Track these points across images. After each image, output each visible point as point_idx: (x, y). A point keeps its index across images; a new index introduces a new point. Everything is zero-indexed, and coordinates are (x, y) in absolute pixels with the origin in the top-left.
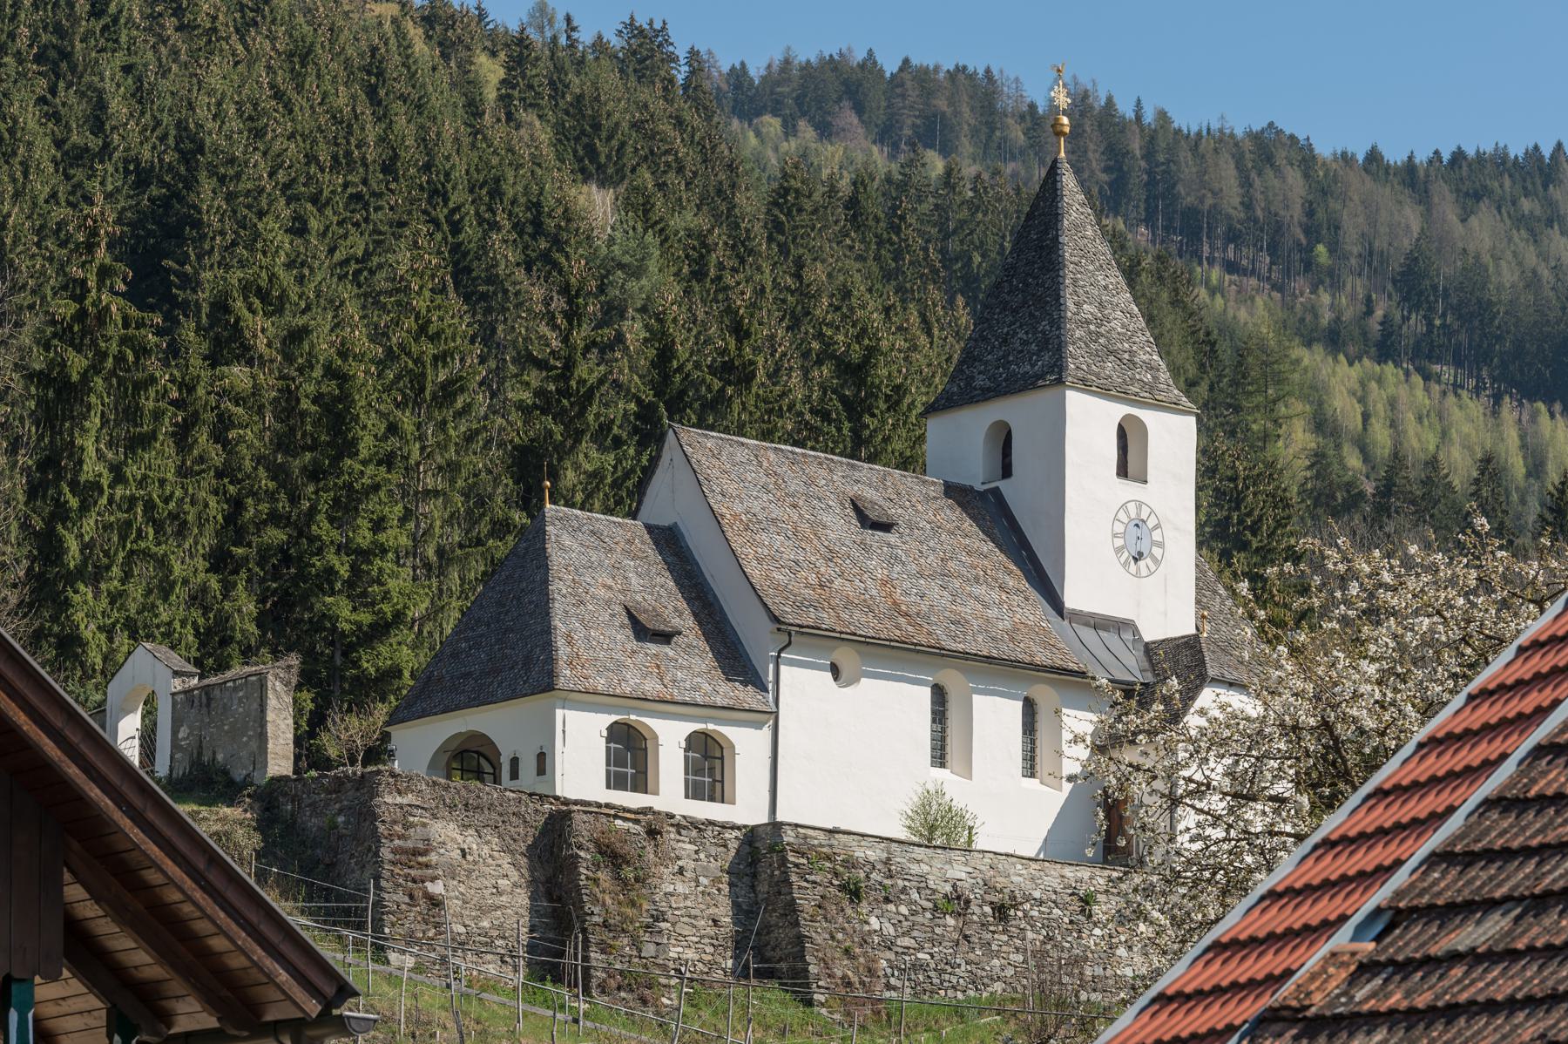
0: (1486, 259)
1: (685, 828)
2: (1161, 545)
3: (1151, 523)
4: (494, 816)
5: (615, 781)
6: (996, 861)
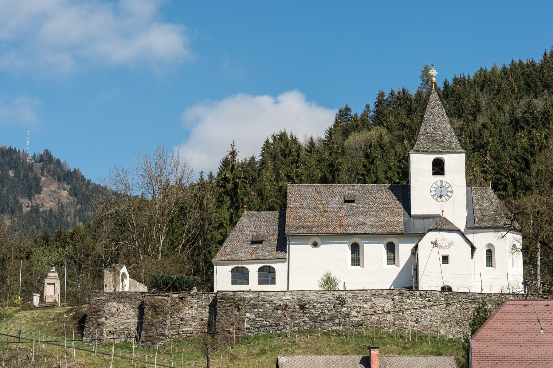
0: (61, 177)
1: (194, 295)
2: (452, 192)
3: (447, 186)
4: (129, 299)
5: (234, 283)
6: (304, 293)
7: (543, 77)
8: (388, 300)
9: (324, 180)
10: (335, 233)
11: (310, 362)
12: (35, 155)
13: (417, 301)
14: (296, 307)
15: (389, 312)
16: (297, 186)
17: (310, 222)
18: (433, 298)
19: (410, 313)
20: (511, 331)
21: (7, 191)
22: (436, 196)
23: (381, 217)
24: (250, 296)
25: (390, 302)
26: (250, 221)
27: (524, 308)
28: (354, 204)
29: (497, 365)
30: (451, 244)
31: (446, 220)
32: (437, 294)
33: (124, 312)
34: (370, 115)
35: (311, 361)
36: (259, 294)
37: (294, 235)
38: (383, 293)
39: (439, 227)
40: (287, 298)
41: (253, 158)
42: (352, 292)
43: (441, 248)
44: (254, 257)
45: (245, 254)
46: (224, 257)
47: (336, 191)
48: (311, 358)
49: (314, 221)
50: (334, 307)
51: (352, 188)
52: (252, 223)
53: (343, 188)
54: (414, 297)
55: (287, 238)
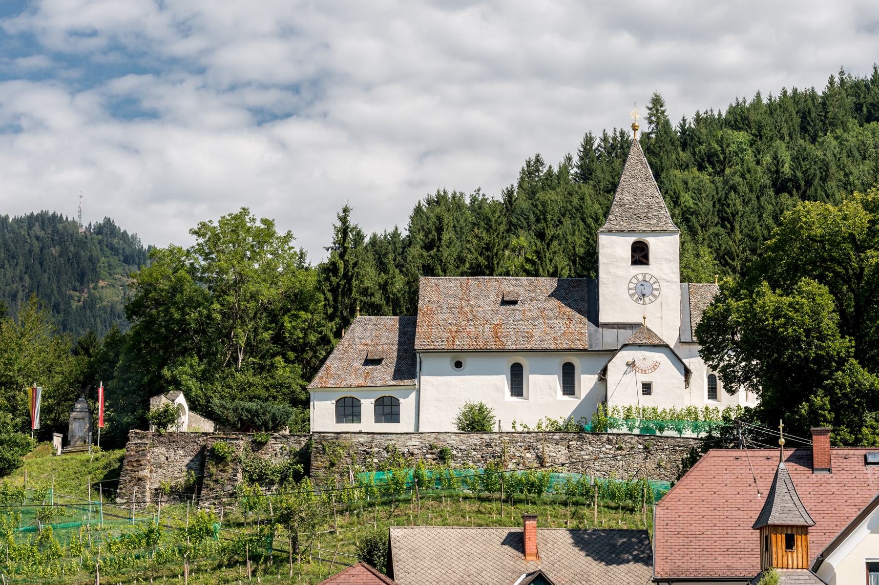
1: (279, 438)
2: (659, 289)
3: (651, 282)
5: (339, 420)
7: (826, 117)
8: (561, 447)
9: (476, 271)
11: (436, 537)
12: (90, 225)
13: (604, 449)
14: (427, 456)
15: (563, 465)
16: (433, 280)
17: (451, 332)
20: (715, 495)
21: (49, 279)
22: (636, 296)
24: (360, 439)
25: (564, 450)
26: (365, 330)
27: (735, 462)
28: (516, 307)
29: (691, 544)
30: (655, 366)
31: (649, 331)
32: (632, 438)
33: (177, 461)
34: (572, 172)
35: (439, 535)
36: (373, 438)
37: (426, 351)
38: (554, 437)
40: (414, 443)
41: (395, 234)
43: (640, 371)
44: (369, 384)
45: (357, 378)
46: (325, 382)
47: (492, 288)
48: (439, 531)
49: (456, 332)
50: (482, 457)
51: (514, 283)
52: (368, 334)
53: (502, 283)
55: (418, 355)
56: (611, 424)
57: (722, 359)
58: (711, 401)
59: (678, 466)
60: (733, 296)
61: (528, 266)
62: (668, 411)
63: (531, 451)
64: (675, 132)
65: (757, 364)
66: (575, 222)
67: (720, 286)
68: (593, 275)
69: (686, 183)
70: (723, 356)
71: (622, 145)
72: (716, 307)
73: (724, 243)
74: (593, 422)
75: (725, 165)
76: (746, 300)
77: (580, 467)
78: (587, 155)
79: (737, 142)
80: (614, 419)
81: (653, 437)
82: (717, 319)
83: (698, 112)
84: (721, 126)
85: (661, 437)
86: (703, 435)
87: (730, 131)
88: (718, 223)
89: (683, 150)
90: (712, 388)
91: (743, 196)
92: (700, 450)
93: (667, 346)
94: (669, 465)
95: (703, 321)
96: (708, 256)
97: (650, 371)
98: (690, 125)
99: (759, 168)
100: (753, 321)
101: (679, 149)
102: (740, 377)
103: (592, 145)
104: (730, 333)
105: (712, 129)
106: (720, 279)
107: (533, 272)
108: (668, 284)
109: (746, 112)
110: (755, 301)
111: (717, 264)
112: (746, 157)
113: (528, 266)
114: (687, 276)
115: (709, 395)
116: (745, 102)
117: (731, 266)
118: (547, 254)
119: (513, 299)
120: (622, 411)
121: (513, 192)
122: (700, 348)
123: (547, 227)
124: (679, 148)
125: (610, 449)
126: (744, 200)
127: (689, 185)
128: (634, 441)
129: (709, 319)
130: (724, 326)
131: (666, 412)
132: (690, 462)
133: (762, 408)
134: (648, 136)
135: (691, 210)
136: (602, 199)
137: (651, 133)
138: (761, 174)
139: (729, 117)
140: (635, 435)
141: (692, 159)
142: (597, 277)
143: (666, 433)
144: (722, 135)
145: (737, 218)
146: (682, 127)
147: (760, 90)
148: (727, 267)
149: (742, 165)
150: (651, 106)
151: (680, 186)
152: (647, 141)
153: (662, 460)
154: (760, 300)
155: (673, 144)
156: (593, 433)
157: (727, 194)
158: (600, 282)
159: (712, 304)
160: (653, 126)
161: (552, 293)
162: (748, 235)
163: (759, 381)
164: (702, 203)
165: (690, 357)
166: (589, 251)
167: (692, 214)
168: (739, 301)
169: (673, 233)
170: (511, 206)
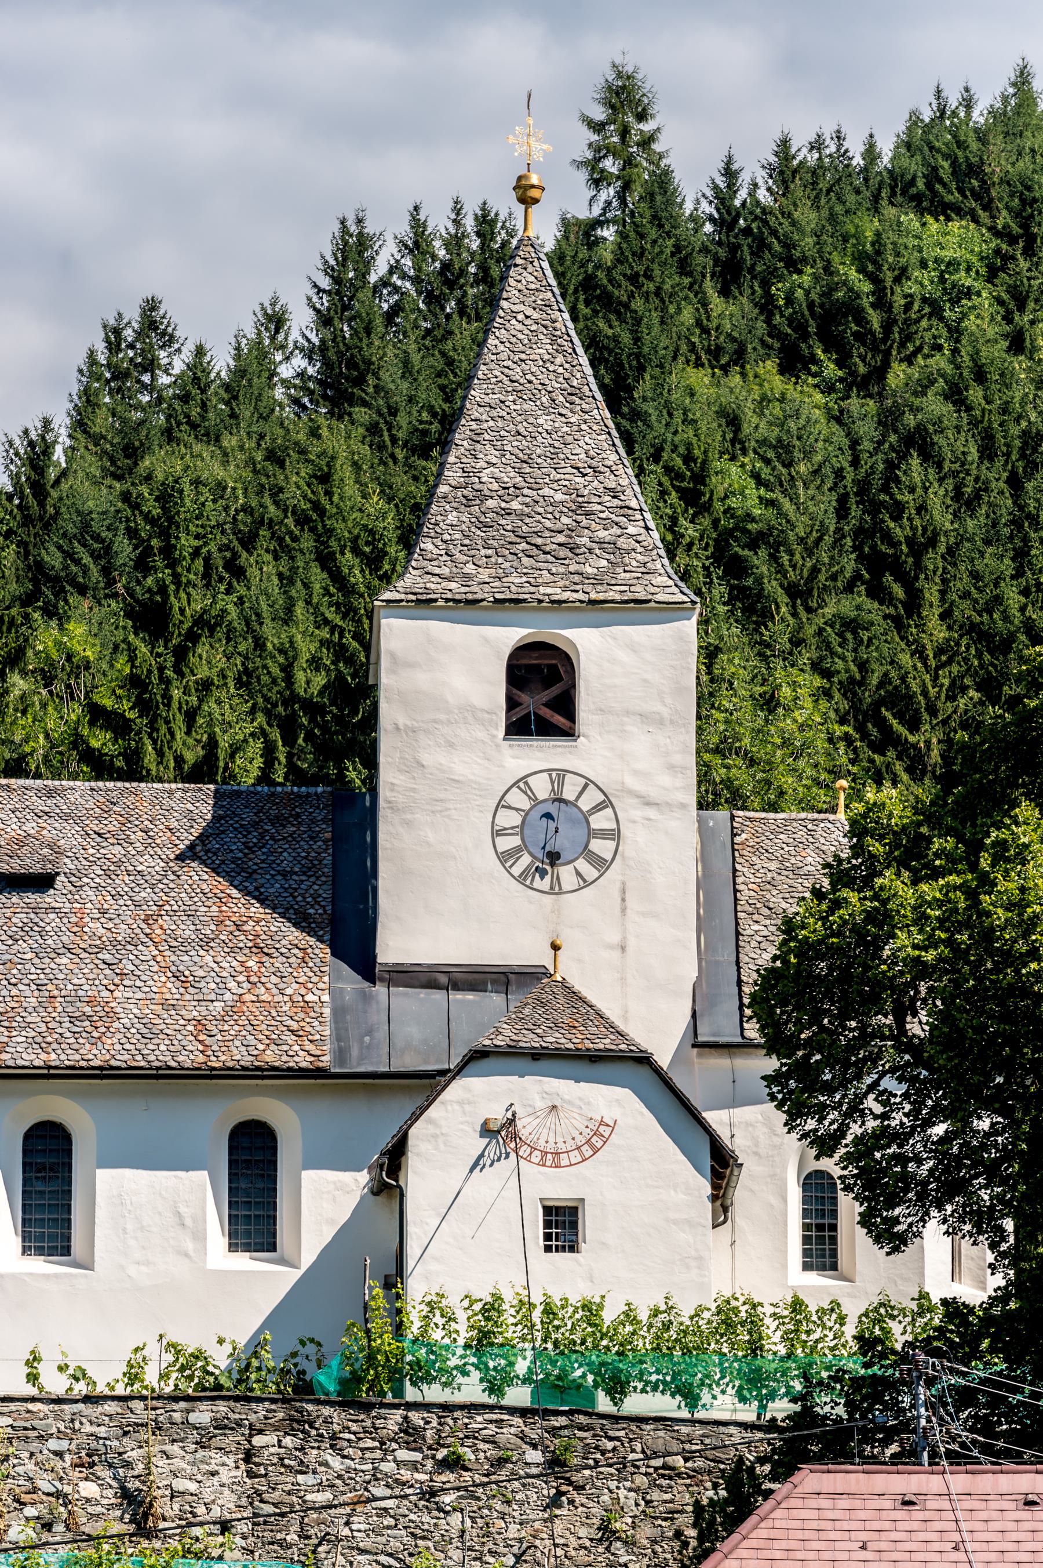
2: (614, 835)
3: (585, 804)
8: (217, 1457)
10: (151, 1069)
13: (388, 1467)
15: (225, 1526)
18: (482, 1446)
19: (346, 1532)
22: (526, 860)
23: (201, 973)
28: (49, 898)
31: (574, 996)
32: (499, 1423)
34: (286, 371)
38: (193, 1418)
39: (529, 1041)
42: (13, 1406)
43: (536, 1157)
51: (40, 805)
54: (370, 1443)
56: (417, 1364)
57: (855, 1110)
58: (814, 1279)
59: (678, 1534)
60: (903, 863)
61: (99, 740)
62: (644, 1316)
63: (99, 1470)
64: (693, 218)
65: (994, 1130)
66: (294, 570)
67: (853, 822)
68: (354, 775)
69: (733, 421)
70: (861, 1098)
71: (483, 268)
72: (837, 904)
73: (880, 660)
74: (347, 1359)
75: (887, 353)
76: (953, 879)
77: (292, 1538)
78: (345, 308)
79: (937, 260)
80: (431, 1348)
81: (582, 1419)
82: (838, 950)
83: (784, 143)
84: (876, 198)
85: (615, 1419)
86: (781, 1408)
87: (910, 219)
88: (857, 577)
89: (725, 292)
90: (820, 1227)
91: (955, 474)
92: (767, 1468)
93: (644, 1060)
94: (645, 1533)
95: (782, 957)
96: (808, 703)
97: (575, 1157)
98: (752, 194)
99: (1019, 365)
100: (980, 962)
101: (710, 287)
102: (924, 1183)
103: (365, 267)
104: (888, 1006)
105: (839, 209)
106: (856, 794)
107: (120, 763)
108: (652, 813)
109: (974, 146)
110: (986, 882)
111: (847, 738)
112: (971, 323)
113: (99, 740)
114: (728, 783)
115: (806, 1253)
116: (968, 104)
117: (904, 750)
118: (176, 693)
119: (37, 869)
120: (462, 1316)
121: (47, 450)
122: (772, 1064)
123: (178, 583)
124: (708, 284)
125: (414, 1466)
126: (958, 489)
127: (746, 429)
128: (507, 1435)
129: (808, 951)
130: (863, 980)
131: (634, 1321)
132: (726, 1516)
133: (1013, 1305)
134: (587, 235)
135: (752, 527)
136: (400, 479)
137: (597, 223)
138: (1030, 389)
139: (905, 162)
140: (512, 1411)
141: (761, 327)
142: (372, 784)
143: (636, 1403)
144: (878, 234)
145: (933, 560)
146: (722, 198)
147: (1031, 60)
148: (891, 754)
149: (955, 351)
150: (599, 114)
151: (710, 432)
152: (583, 254)
153: (617, 1508)
154: (1006, 876)
155: (684, 267)
156: (346, 1403)
157: (891, 466)
158: (382, 803)
159: (818, 894)
160: (608, 193)
161: (191, 847)
162: (971, 629)
163: (1000, 1198)
164: (794, 499)
165: (734, 1102)
166: (340, 677)
167: (753, 545)
168: (928, 878)
169: (670, 611)
170: (42, 504)
